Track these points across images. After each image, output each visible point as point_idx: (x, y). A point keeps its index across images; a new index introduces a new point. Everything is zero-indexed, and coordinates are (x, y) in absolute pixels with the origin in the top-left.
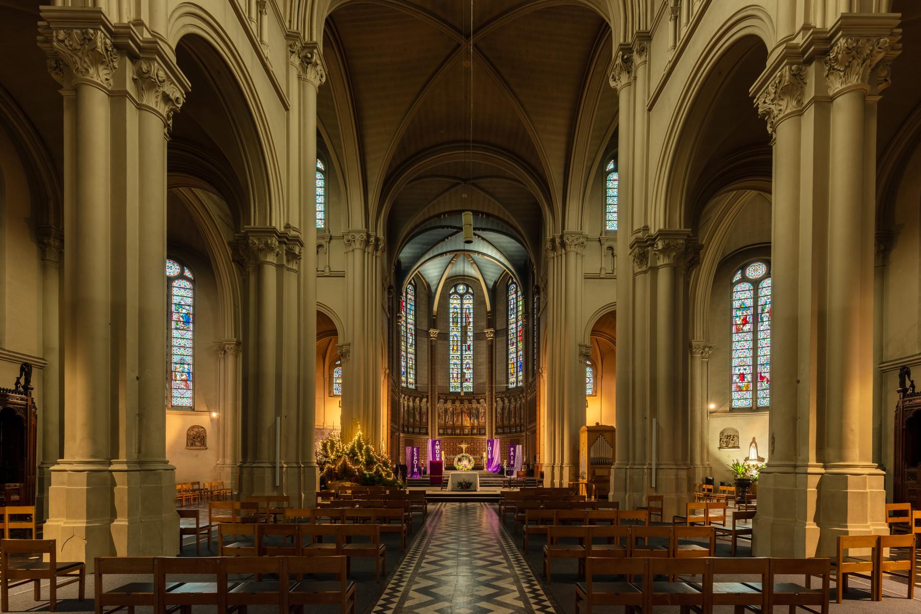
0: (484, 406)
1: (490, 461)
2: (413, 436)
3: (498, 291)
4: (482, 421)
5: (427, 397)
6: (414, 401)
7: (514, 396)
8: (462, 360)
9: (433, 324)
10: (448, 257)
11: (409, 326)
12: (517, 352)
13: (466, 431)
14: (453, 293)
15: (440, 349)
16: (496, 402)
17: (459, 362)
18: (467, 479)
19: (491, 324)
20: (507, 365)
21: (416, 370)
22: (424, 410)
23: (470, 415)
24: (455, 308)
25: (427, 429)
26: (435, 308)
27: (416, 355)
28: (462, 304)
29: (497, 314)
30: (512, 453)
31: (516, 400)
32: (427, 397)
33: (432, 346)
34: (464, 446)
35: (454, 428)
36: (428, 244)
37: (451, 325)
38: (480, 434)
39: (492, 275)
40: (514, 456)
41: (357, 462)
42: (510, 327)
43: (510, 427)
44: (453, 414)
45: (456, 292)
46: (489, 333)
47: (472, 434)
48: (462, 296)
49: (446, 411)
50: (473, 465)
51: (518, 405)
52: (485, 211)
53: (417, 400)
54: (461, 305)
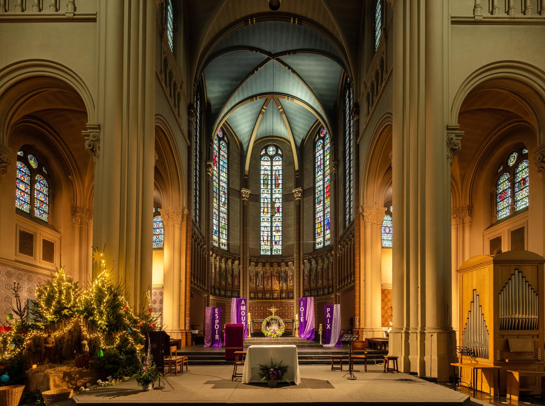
0: (292, 269)
1: (303, 325)
3: (306, 149)
4: (290, 284)
5: (239, 261)
6: (226, 262)
7: (321, 257)
8: (272, 222)
9: (245, 184)
10: (259, 102)
11: (222, 184)
12: (324, 211)
13: (276, 295)
14: (264, 155)
15: (251, 211)
16: (304, 264)
17: (268, 224)
18: (277, 360)
19: (299, 183)
21: (228, 230)
22: (236, 272)
23: (279, 278)
24: (265, 170)
25: (239, 292)
26: (247, 168)
27: (228, 215)
28: (272, 166)
30: (328, 315)
34: (273, 310)
35: (264, 292)
36: (236, 79)
37: (262, 186)
38: (289, 298)
39: (302, 128)
40: (331, 319)
41: (92, 326)
42: (317, 185)
43: (317, 289)
44: (263, 277)
45: (266, 154)
46: (297, 192)
47: (281, 298)
48: (272, 157)
49: (257, 274)
50: (283, 330)
51: (325, 266)
52: (298, 12)
53: (230, 262)
54: (271, 167)
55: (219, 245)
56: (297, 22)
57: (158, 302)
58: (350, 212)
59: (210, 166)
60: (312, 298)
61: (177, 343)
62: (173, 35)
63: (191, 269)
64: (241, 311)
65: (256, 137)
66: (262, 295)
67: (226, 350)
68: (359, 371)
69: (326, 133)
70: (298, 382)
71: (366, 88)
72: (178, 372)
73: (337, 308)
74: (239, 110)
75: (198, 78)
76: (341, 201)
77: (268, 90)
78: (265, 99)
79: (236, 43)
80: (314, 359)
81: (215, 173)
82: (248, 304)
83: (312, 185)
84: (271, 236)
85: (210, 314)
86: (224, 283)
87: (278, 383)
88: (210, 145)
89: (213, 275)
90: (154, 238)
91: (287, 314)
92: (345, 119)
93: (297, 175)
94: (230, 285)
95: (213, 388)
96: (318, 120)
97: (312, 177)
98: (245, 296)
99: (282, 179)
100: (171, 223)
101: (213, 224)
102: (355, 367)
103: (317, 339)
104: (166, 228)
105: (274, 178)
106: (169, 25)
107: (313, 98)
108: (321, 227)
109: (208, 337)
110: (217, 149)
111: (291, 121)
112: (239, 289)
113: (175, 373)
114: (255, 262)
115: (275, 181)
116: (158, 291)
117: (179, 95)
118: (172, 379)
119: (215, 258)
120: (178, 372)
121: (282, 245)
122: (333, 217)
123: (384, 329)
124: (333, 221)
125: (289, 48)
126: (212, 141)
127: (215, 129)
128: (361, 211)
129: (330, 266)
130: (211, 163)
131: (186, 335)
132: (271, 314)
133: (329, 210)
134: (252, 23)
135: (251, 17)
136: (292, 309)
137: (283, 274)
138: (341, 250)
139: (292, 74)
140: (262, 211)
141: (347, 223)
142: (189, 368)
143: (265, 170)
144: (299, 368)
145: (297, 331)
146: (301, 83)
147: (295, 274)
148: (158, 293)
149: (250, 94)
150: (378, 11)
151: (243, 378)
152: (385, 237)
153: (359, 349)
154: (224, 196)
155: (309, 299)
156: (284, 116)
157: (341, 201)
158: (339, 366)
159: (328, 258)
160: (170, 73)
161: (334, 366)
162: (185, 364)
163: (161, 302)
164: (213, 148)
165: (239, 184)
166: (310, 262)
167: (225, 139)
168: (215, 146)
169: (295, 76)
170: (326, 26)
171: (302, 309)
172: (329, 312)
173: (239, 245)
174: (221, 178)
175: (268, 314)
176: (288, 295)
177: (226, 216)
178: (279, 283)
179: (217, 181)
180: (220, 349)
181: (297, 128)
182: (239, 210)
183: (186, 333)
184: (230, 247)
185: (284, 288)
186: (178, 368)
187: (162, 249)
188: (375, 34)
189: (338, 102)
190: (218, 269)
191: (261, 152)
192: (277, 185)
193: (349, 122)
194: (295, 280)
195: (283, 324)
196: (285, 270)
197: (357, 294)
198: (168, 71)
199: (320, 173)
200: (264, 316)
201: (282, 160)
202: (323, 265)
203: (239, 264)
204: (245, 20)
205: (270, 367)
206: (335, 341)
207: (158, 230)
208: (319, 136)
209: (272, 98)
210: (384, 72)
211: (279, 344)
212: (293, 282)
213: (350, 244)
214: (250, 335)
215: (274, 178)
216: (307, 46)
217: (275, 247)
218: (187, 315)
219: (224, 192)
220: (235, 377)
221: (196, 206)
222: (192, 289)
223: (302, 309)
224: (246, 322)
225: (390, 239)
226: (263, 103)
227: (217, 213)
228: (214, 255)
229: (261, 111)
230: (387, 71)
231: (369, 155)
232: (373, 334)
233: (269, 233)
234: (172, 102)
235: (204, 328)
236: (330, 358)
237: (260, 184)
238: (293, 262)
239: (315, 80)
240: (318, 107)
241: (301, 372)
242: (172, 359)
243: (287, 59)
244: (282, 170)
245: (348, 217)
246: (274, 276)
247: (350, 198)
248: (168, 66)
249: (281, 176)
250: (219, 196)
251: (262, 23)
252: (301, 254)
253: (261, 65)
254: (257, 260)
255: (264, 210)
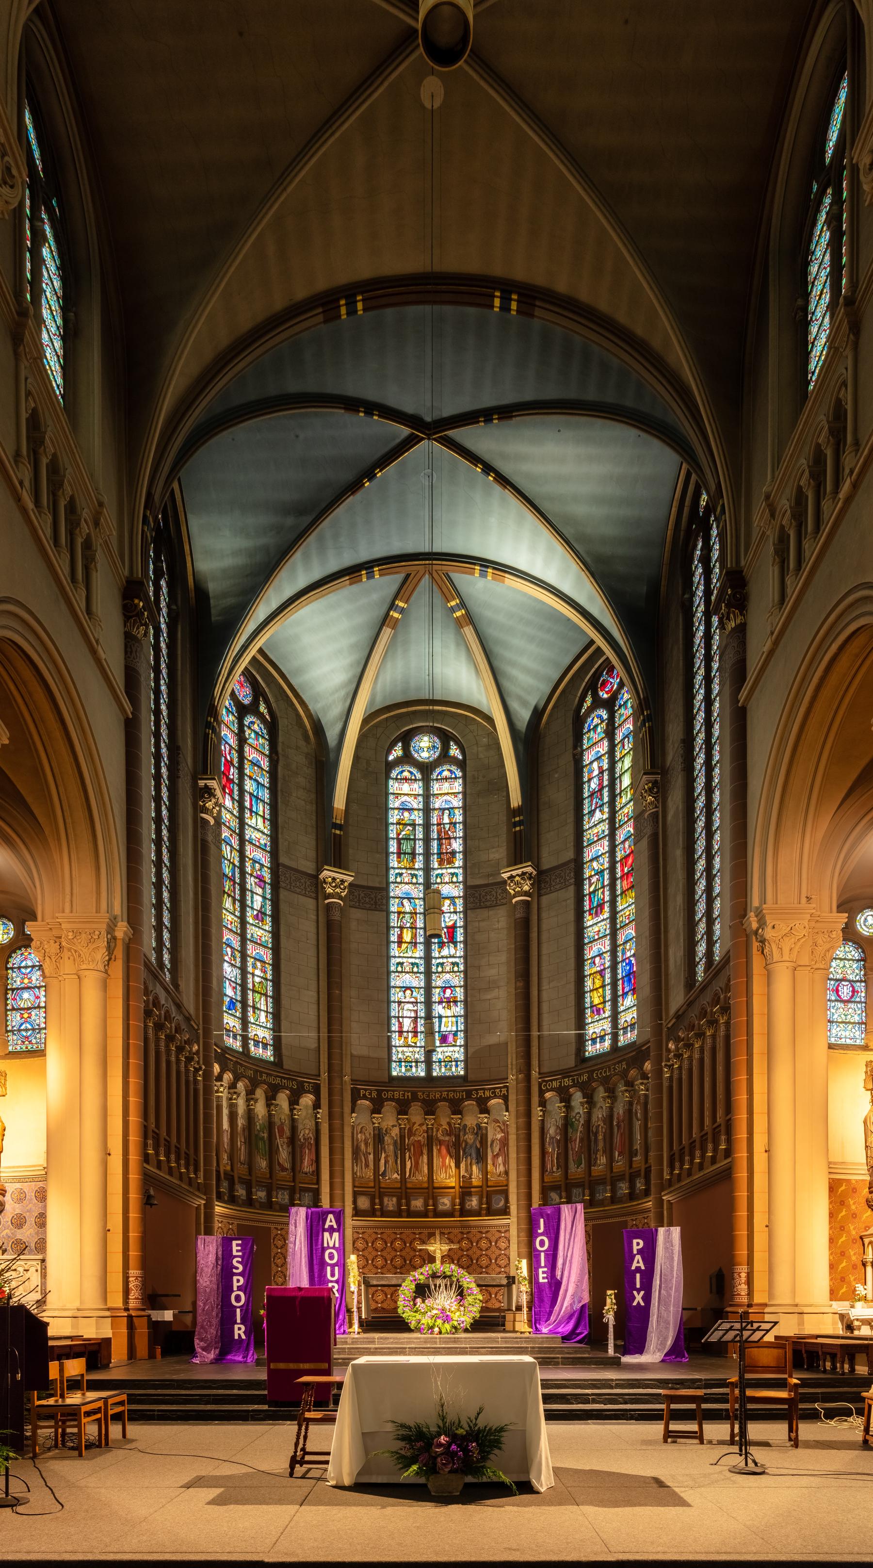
0: (501, 1120)
1: (545, 1296)
2: (269, 1216)
3: (548, 740)
4: (496, 1168)
6: (270, 1099)
7: (605, 1081)
8: (428, 974)
9: (333, 851)
10: (383, 585)
13: (445, 1203)
14: (398, 762)
15: (356, 935)
16: (543, 1103)
17: (418, 982)
18: (463, 1404)
19: (522, 848)
20: (580, 979)
21: (277, 999)
22: (305, 1131)
23: (457, 1150)
25: (316, 1194)
26: (340, 801)
28: (427, 796)
29: (544, 816)
30: (638, 1262)
31: (612, 1093)
32: (316, 1091)
33: (329, 925)
34: (437, 1248)
35: (404, 1192)
36: (298, 509)
37: (393, 862)
38: (490, 1212)
39: (534, 674)
40: (648, 1275)
42: (588, 854)
43: (591, 1184)
44: (401, 1147)
45: (407, 758)
46: (517, 880)
47: (464, 1212)
49: (379, 1137)
51: (620, 1109)
52: (519, 273)
53: (283, 1099)
54: (425, 799)
55: (245, 1044)
56: (514, 306)
57: (31, 1221)
58: (709, 932)
59: (208, 792)
60: (580, 1207)
61: (95, 1353)
62: (65, 347)
63: (145, 1115)
64: (324, 1250)
65: (372, 701)
66: (399, 1204)
67: (270, 1372)
68: (766, 1444)
69: (621, 685)
70: (544, 1481)
71: (773, 515)
72: (89, 1446)
73: (670, 1240)
74: (308, 613)
75: (157, 498)
76: (677, 901)
77: (410, 547)
78: (400, 577)
79: (293, 386)
80: (594, 1401)
81: (226, 816)
82: (349, 1232)
83: (570, 855)
84: (429, 1017)
85: (212, 1258)
86: (264, 1164)
87: (467, 1485)
88: (209, 725)
89: (226, 1139)
90: (15, 1019)
91: (484, 1262)
92: (689, 636)
93: (515, 824)
94: (284, 1169)
95: (216, 1501)
96: (592, 642)
97: (570, 829)
98: (337, 1198)
99: (465, 838)
100: (68, 966)
101: (222, 978)
102: (756, 1430)
103: (595, 1337)
104: (54, 982)
105: (435, 835)
106: (46, 313)
107: (574, 567)
108: (603, 986)
109: (207, 1330)
110: (232, 741)
111: (497, 650)
112: (318, 1182)
113: (78, 1448)
114: (371, 1100)
115: (440, 845)
116: (30, 1189)
117: (88, 545)
118: (65, 1470)
119: (233, 1086)
120: (89, 1446)
121: (466, 1046)
122: (647, 953)
123: (840, 1306)
124: (648, 967)
125: (488, 400)
126: (213, 712)
127: (225, 672)
128: (755, 925)
129: (638, 1110)
130: (213, 784)
131: (131, 1326)
132: (432, 1260)
133: (631, 931)
134: (352, 312)
135: (349, 291)
136: (502, 1245)
137: (470, 1138)
138: (678, 1056)
139: (497, 488)
140: (394, 938)
141: (700, 969)
142: (133, 1430)
143: (403, 809)
144: (546, 1430)
145: (524, 1315)
146: (530, 519)
147: (512, 1139)
148: (31, 1195)
149: (348, 559)
150: (818, 253)
151: (330, 1467)
152: (837, 1012)
153: (767, 1369)
154: (259, 891)
155: (566, 1211)
156: (468, 631)
157: (677, 901)
158: (694, 1427)
159: (630, 1084)
160: (54, 468)
161: (673, 1427)
162: (117, 1417)
163: (42, 1221)
164: (220, 739)
165: (312, 854)
166: (566, 1099)
167: (262, 708)
168: (225, 732)
169: (508, 494)
170: (622, 317)
171: (542, 1243)
172: (640, 1252)
173: (313, 1045)
174: (249, 833)
175: (418, 1261)
176: (488, 1203)
177: (267, 956)
178: (458, 1166)
179: (235, 843)
180: (249, 1369)
181: (514, 672)
182: (312, 936)
183: (130, 1317)
184: (284, 1052)
185: (476, 1182)
186: (91, 1430)
187: (41, 1053)
188: (806, 332)
189: (664, 582)
190: (241, 1122)
191: (389, 752)
192: (447, 858)
193: (708, 635)
194: (513, 1155)
195: (476, 1290)
196: (479, 1126)
197: (742, 1194)
198: (44, 461)
199: (598, 815)
200: (408, 1266)
201: (464, 777)
202: (611, 1109)
203: (317, 1105)
204: (326, 302)
205: (434, 1429)
206: (663, 1344)
207: (26, 995)
208: (595, 695)
209: (427, 572)
210: (849, 448)
211: (463, 1352)
212: (506, 1162)
213: (714, 1036)
214: (356, 1327)
215: (435, 835)
216: (551, 392)
217: (441, 1052)
218: (132, 1262)
219: (260, 878)
220: (302, 1462)
221: (159, 917)
222: (147, 1179)
223: (542, 1243)
224: (343, 1283)
225: (857, 1019)
226: (394, 588)
227: (236, 944)
228: (228, 1077)
229: (387, 614)
230: (857, 443)
231: (783, 739)
232: (801, 1323)
233: (421, 1007)
234: (63, 567)
235: (194, 1304)
236: (656, 1398)
237: (387, 854)
238: (506, 1098)
239: (581, 510)
240: (591, 599)
241: (553, 1448)
242: (69, 1401)
243: (481, 439)
244: (465, 808)
245: (701, 949)
246: (440, 1143)
247: (709, 889)
248: (61, 484)
249: (460, 827)
250: (243, 890)
251: (389, 312)
252: (535, 1074)
253: (385, 461)
254: (379, 1092)
255: (400, 937)
